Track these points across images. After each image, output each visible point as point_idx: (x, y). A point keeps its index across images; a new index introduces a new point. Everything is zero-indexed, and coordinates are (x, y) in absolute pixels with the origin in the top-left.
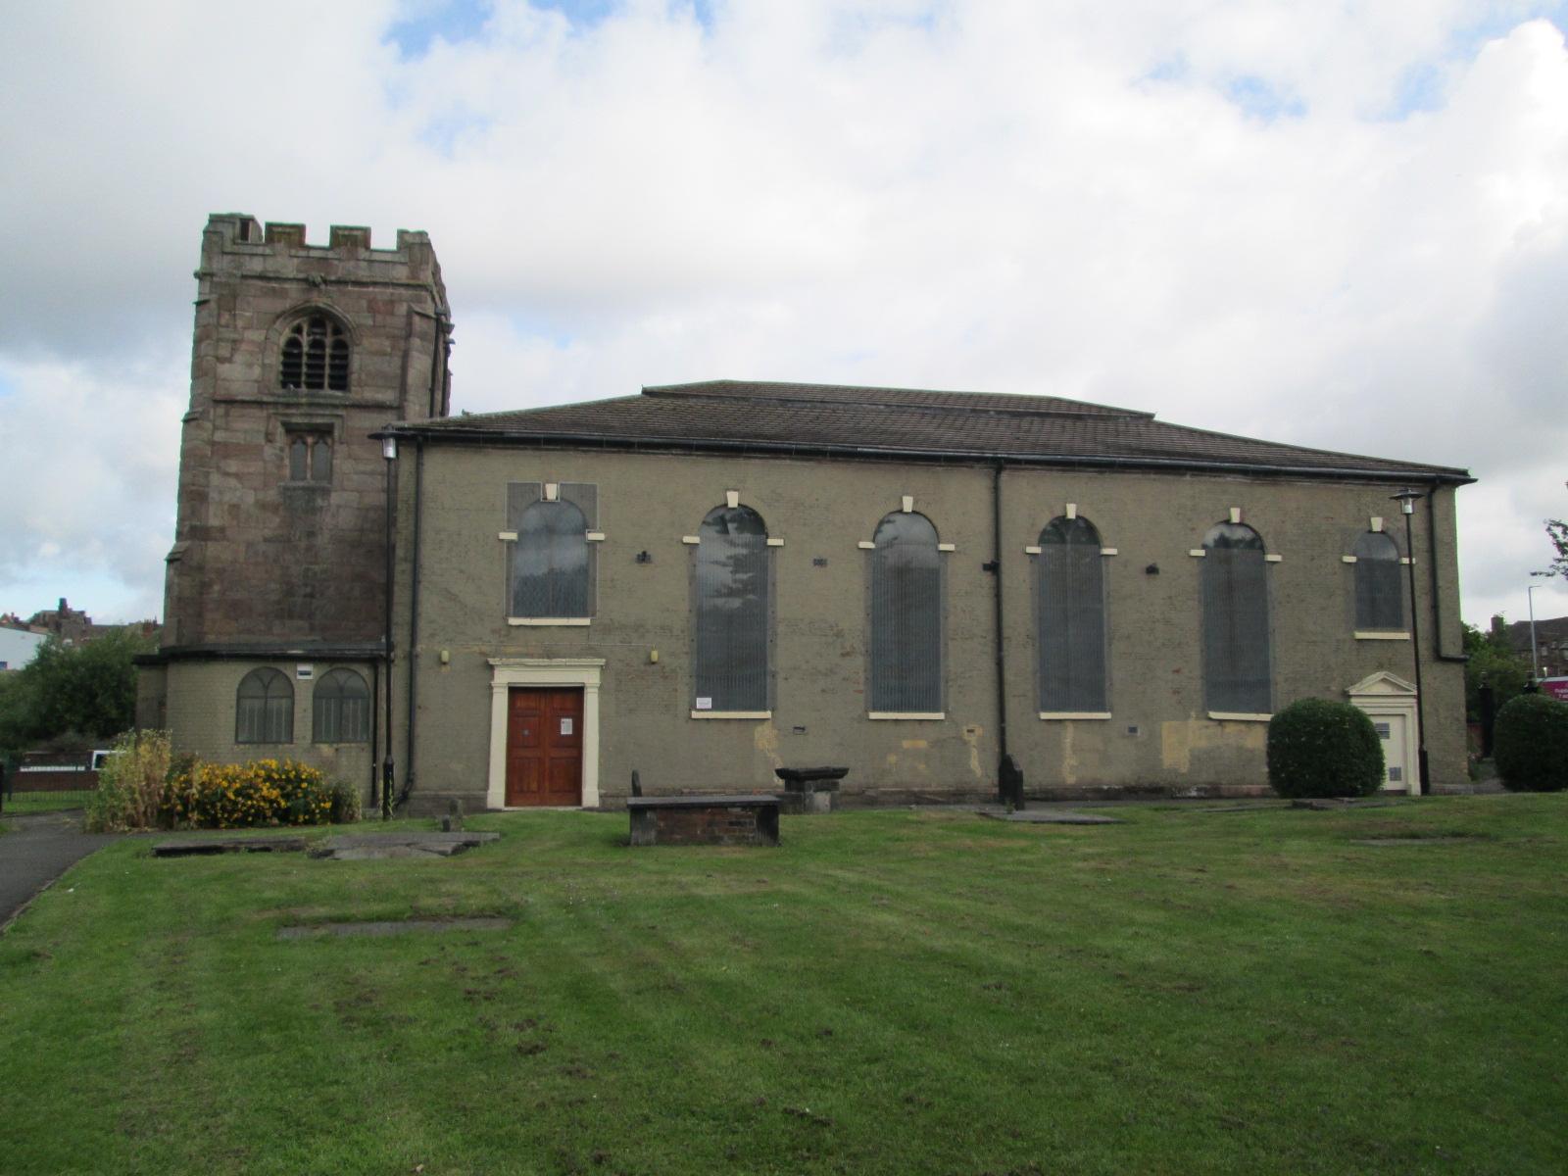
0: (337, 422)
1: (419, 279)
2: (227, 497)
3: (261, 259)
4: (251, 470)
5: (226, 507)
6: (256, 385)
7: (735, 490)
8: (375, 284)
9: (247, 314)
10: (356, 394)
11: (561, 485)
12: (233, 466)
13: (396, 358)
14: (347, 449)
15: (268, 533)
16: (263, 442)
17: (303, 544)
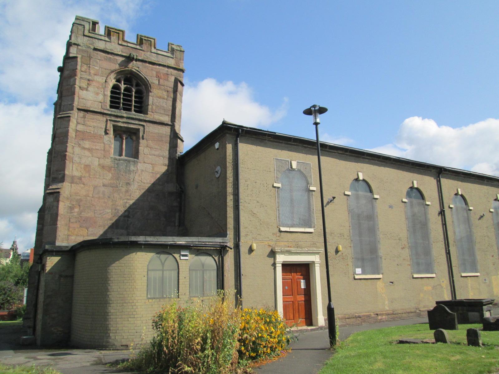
0: (141, 128)
1: (179, 66)
2: (83, 161)
3: (104, 42)
4: (97, 147)
5: (83, 166)
6: (100, 104)
7: (361, 172)
8: (160, 65)
9: (96, 68)
10: (150, 116)
11: (297, 162)
12: (87, 144)
13: (170, 102)
14: (146, 142)
15: (106, 182)
16: (104, 134)
17: (124, 189)
